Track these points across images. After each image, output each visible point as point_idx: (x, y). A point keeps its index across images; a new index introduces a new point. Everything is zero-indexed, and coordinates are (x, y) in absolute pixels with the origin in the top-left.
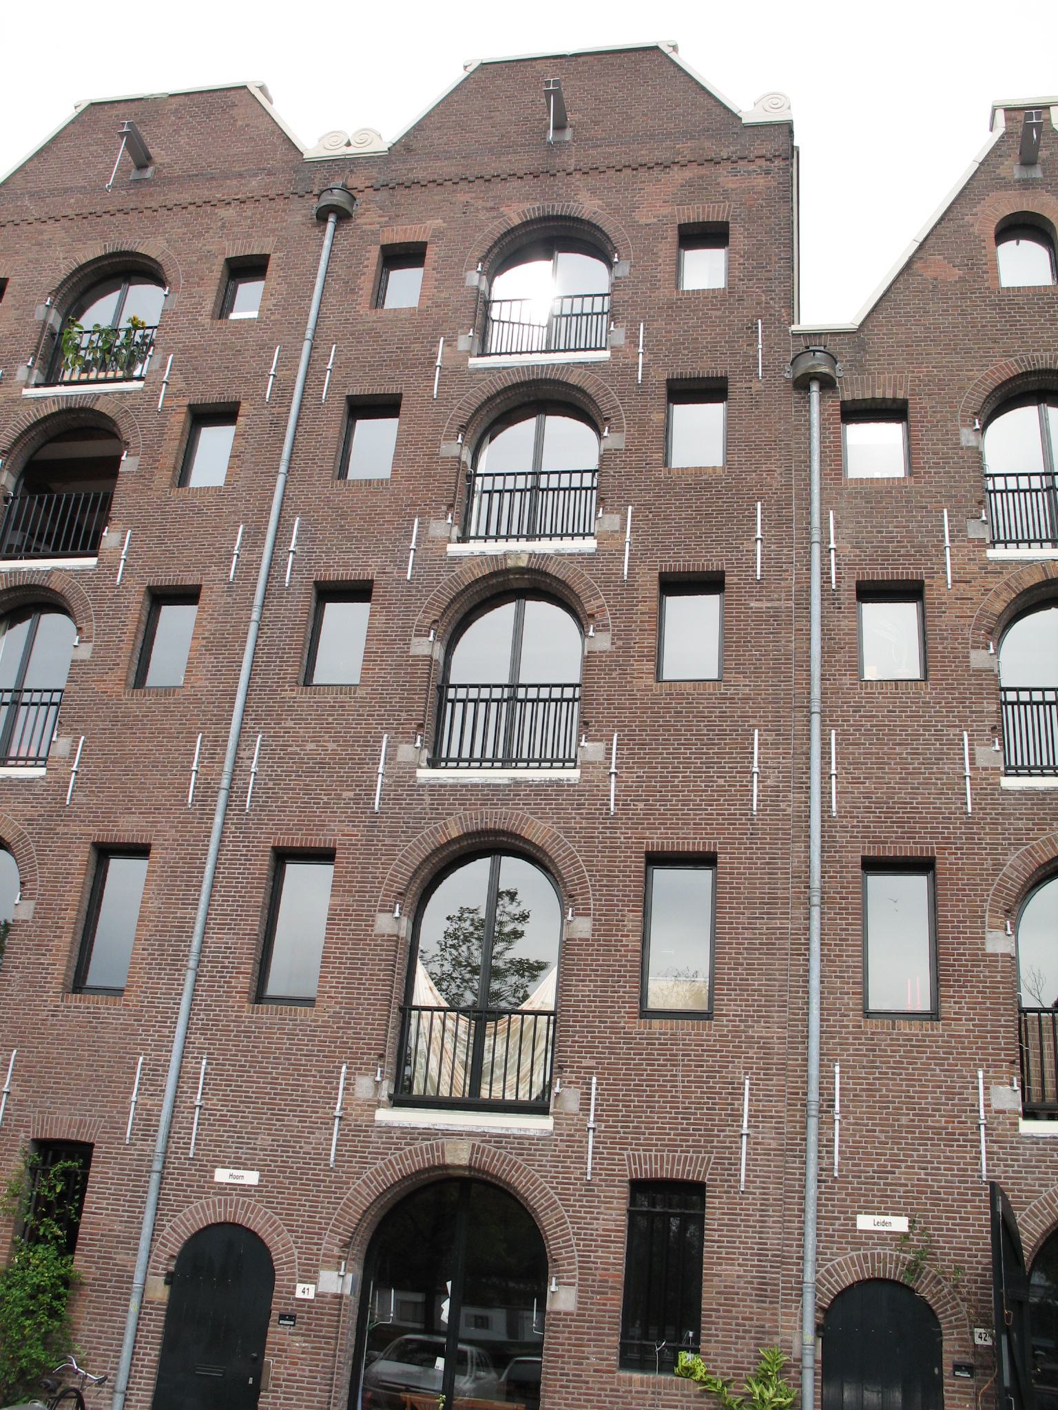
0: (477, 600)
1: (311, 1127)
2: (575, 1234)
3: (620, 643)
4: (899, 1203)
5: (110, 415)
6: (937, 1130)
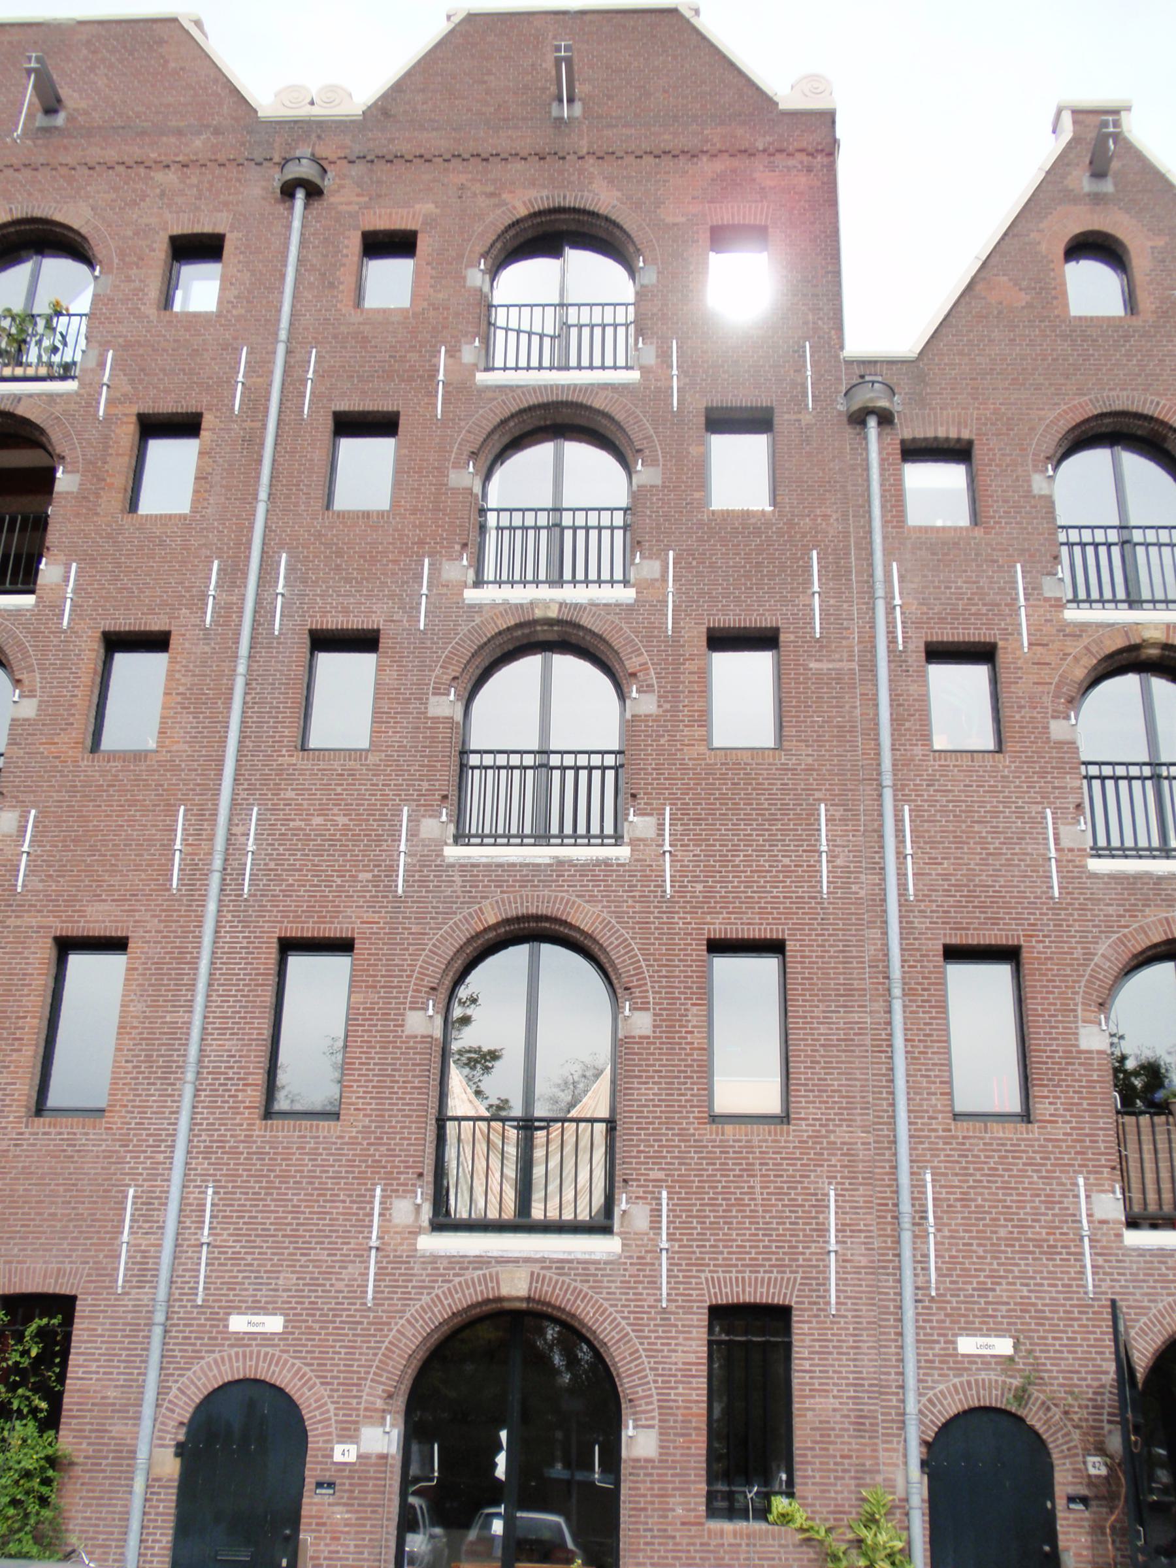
0: (499, 654)
1: (342, 1261)
2: (651, 1369)
3: (667, 706)
4: (1002, 1323)
5: (38, 421)
6: (1038, 1243)
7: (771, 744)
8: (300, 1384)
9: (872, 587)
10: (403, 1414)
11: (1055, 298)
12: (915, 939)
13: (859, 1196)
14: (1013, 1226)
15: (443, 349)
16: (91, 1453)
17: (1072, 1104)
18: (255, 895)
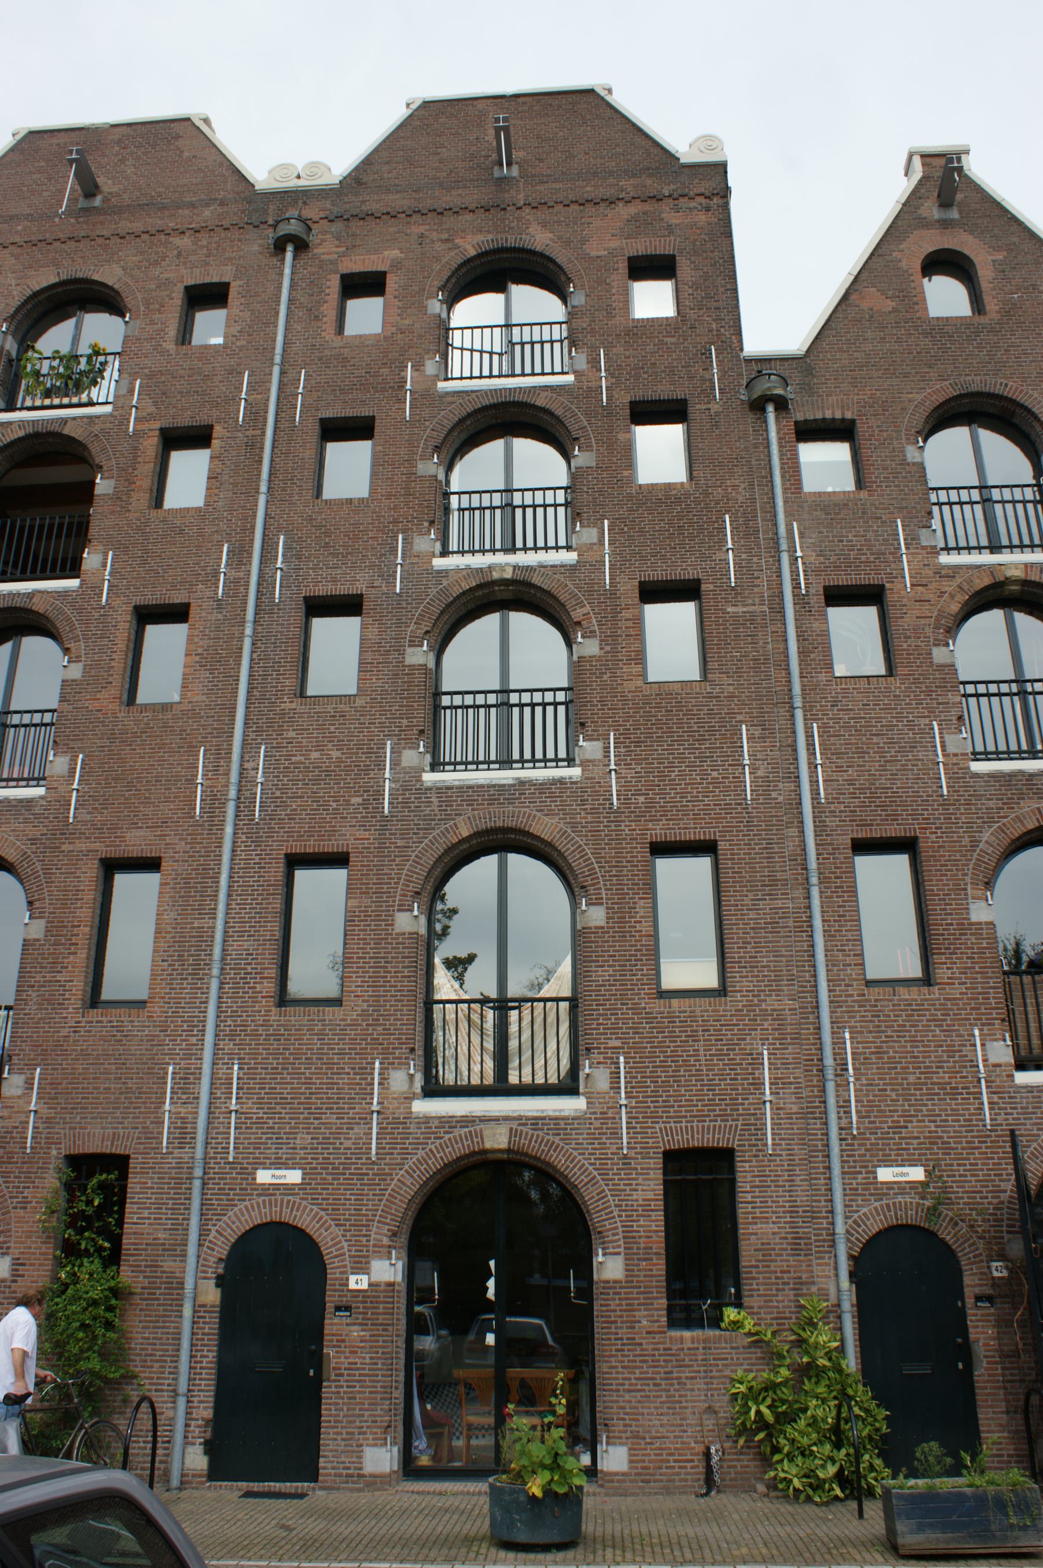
1: (349, 1123)
2: (616, 1206)
3: (608, 648)
4: (914, 1154)
6: (942, 1086)
7: (697, 677)
8: (318, 1226)
9: (777, 543)
10: (406, 1249)
11: (917, 304)
12: (827, 835)
13: (789, 1054)
14: (920, 1073)
15: (410, 365)
16: (147, 1285)
17: (966, 968)
18: (265, 819)
